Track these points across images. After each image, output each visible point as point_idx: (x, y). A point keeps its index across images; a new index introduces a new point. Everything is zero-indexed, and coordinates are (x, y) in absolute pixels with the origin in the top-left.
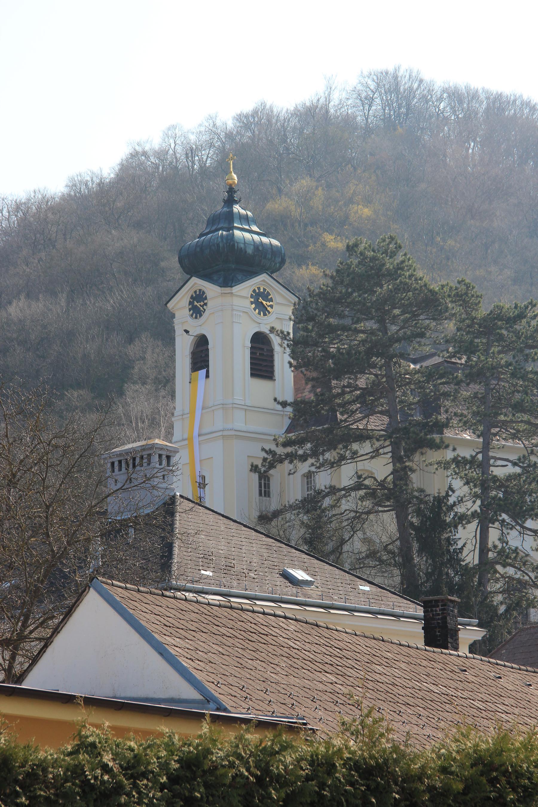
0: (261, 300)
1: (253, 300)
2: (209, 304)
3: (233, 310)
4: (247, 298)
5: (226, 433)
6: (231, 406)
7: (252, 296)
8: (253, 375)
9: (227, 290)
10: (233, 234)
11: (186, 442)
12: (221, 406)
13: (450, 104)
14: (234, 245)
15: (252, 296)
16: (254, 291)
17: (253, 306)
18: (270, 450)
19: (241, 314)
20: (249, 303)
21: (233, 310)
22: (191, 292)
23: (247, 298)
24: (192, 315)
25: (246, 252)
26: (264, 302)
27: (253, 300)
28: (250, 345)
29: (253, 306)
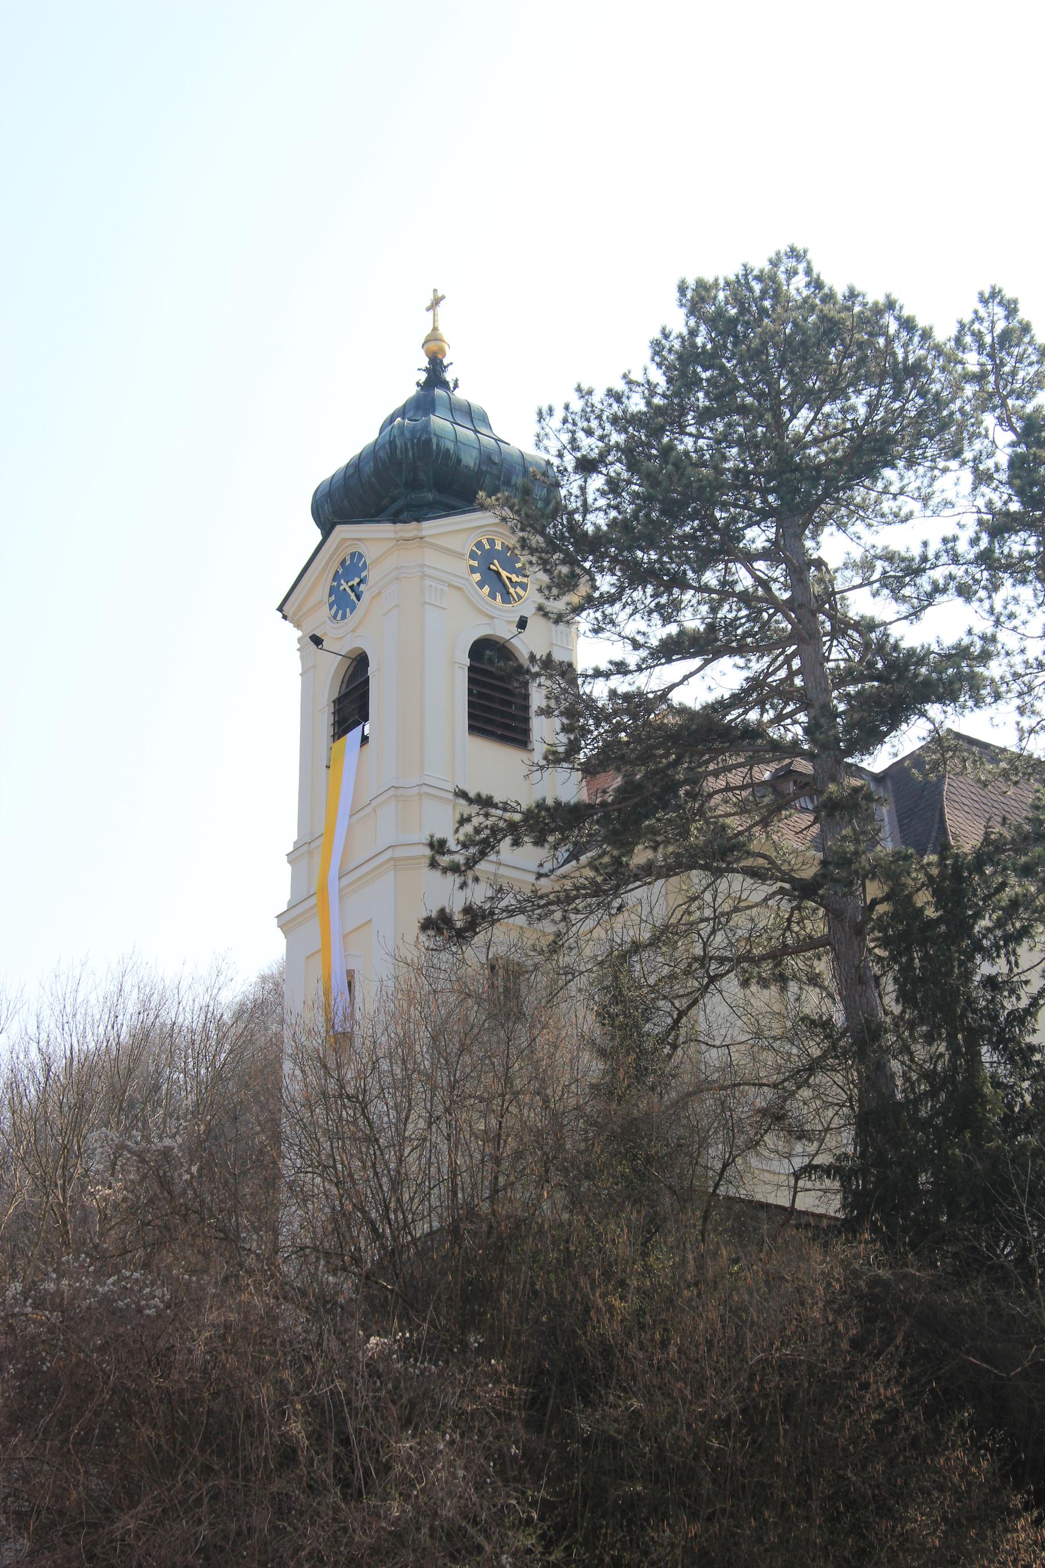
0: (496, 566)
1: (475, 563)
2: (371, 581)
3: (424, 576)
4: (460, 556)
5: (400, 853)
6: (416, 790)
7: (473, 555)
8: (473, 729)
9: (409, 529)
10: (427, 424)
11: (313, 901)
12: (392, 792)
13: (863, 1041)
14: (428, 442)
15: (473, 555)
16: (479, 545)
17: (477, 577)
18: (479, 795)
19: (446, 589)
20: (464, 571)
21: (424, 576)
22: (335, 566)
23: (460, 556)
24: (335, 617)
25: (459, 461)
26: (504, 574)
27: (475, 563)
28: (467, 662)
29: (477, 577)
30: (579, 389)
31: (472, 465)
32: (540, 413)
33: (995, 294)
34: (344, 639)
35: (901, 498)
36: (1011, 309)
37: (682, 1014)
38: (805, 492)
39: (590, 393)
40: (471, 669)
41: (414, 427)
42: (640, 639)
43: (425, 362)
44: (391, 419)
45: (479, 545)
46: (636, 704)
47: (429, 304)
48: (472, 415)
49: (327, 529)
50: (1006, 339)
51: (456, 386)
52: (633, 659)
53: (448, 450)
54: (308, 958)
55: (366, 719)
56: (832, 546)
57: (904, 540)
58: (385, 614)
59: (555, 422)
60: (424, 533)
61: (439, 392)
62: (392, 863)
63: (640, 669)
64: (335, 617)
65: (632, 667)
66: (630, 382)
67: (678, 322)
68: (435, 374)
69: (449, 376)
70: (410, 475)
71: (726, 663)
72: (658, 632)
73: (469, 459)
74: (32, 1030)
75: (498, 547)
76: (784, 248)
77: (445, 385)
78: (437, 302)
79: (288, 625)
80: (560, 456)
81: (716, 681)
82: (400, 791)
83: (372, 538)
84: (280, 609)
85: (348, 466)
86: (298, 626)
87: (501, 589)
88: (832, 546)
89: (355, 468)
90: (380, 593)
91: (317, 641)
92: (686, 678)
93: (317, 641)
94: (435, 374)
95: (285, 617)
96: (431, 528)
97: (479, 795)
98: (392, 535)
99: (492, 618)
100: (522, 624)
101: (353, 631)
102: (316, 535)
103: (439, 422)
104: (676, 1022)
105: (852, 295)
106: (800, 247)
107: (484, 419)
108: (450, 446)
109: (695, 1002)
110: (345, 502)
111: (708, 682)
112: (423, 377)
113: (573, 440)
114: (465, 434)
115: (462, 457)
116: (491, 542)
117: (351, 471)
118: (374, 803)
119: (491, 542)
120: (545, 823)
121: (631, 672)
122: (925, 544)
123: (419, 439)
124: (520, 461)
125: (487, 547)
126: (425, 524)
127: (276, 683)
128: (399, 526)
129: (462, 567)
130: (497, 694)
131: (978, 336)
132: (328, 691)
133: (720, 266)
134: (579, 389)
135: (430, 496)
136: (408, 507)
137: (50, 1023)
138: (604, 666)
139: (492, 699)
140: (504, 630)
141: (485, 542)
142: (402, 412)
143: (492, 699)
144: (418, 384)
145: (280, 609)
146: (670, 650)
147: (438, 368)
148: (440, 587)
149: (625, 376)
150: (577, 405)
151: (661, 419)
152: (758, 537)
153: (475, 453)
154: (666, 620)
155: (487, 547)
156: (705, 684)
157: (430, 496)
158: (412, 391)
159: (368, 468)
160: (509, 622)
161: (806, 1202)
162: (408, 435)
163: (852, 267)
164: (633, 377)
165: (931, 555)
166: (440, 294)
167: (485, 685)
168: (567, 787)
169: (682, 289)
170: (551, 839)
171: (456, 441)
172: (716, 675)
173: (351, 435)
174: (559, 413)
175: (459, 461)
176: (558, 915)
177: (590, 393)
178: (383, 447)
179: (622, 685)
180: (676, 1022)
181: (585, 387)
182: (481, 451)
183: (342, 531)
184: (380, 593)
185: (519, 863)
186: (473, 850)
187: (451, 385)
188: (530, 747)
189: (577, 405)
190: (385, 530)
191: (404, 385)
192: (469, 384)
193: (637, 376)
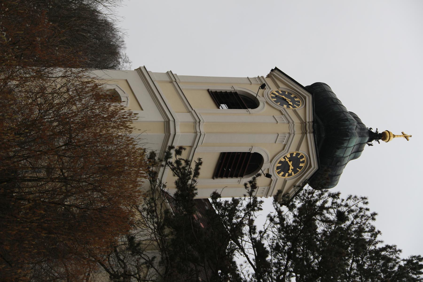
1: (294, 155)
4: (298, 149)
9: (309, 128)
12: (198, 120)
14: (347, 136)
15: (298, 154)
18: (199, 169)
19: (284, 143)
23: (298, 149)
24: (273, 93)
27: (294, 155)
31: (337, 154)
32: (365, 198)
39: (373, 219)
40: (249, 153)
41: (353, 129)
44: (356, 117)
47: (405, 133)
49: (309, 89)
51: (369, 145)
53: (343, 144)
54: (126, 81)
58: (273, 116)
59: (361, 205)
60: (308, 135)
62: (167, 120)
64: (273, 93)
69: (374, 142)
72: (266, 243)
73: (339, 153)
77: (370, 140)
78: (406, 137)
82: (198, 124)
83: (306, 111)
84: (276, 68)
85: (337, 99)
86: (268, 76)
87: (283, 168)
90: (282, 114)
95: (272, 70)
97: (199, 169)
98: (307, 120)
99: (271, 162)
101: (267, 102)
103: (355, 141)
107: (355, 157)
108: (345, 145)
110: (320, 95)
111: (244, 265)
112: (374, 131)
114: (349, 151)
115: (340, 150)
117: (335, 101)
118: (193, 112)
119: (303, 162)
121: (251, 235)
123: (348, 132)
124: (337, 174)
125: (301, 160)
126: (312, 135)
127: (243, 68)
130: (238, 164)
134: (375, 214)
135: (323, 136)
141: (303, 159)
142: (359, 122)
144: (371, 128)
145: (276, 68)
147: (378, 137)
148: (285, 141)
149: (379, 232)
150: (368, 213)
153: (342, 155)
155: (301, 160)
158: (368, 126)
160: (268, 169)
162: (350, 127)
164: (379, 236)
166: (409, 138)
171: (347, 148)
173: (350, 100)
175: (338, 148)
177: (373, 219)
178: (345, 116)
181: (376, 217)
182: (343, 157)
184: (282, 114)
187: (370, 143)
188: (215, 178)
189: (368, 213)
191: (371, 123)
192: (372, 151)
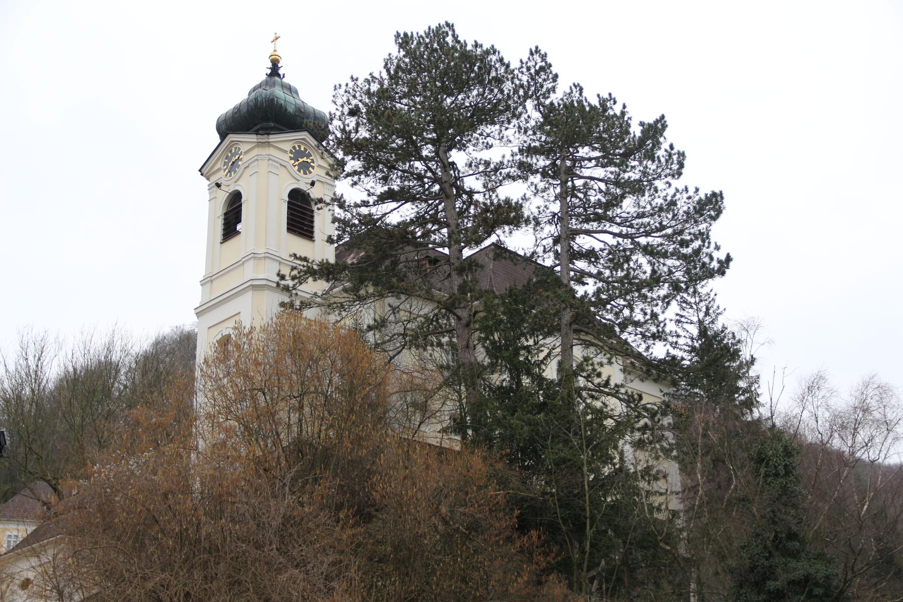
4: (286, 152)
7: (291, 152)
8: (289, 230)
9: (264, 139)
15: (291, 152)
20: (287, 159)
23: (286, 152)
30: (352, 77)
33: (537, 50)
34: (230, 187)
35: (488, 139)
36: (544, 57)
37: (392, 358)
38: (454, 129)
39: (357, 79)
40: (289, 203)
42: (372, 191)
43: (270, 65)
44: (254, 89)
45: (294, 147)
46: (368, 220)
48: (289, 89)
50: (542, 69)
52: (371, 200)
55: (240, 221)
56: (457, 157)
57: (495, 155)
59: (342, 91)
61: (277, 78)
63: (374, 205)
65: (371, 203)
66: (373, 77)
67: (396, 52)
68: (275, 71)
69: (281, 72)
70: (265, 116)
71: (409, 205)
72: (380, 189)
73: (291, 109)
74: (70, 356)
75: (302, 149)
76: (443, 23)
77: (279, 75)
79: (203, 178)
80: (342, 106)
81: (407, 212)
83: (245, 141)
84: (200, 170)
86: (208, 179)
87: (305, 167)
88: (457, 157)
89: (238, 110)
91: (218, 185)
92: (392, 211)
93: (218, 185)
94: (275, 71)
95: (202, 175)
96: (273, 138)
100: (313, 184)
102: (217, 139)
103: (279, 92)
104: (389, 362)
105: (476, 45)
106: (451, 22)
107: (297, 93)
108: (283, 102)
109: (399, 352)
110: (235, 124)
111: (401, 213)
112: (269, 71)
113: (348, 100)
114: (290, 98)
116: (299, 147)
119: (299, 147)
120: (326, 271)
122: (504, 157)
126: (271, 136)
128: (259, 136)
129: (286, 157)
130: (300, 214)
131: (528, 69)
132: (220, 210)
133: (418, 27)
134: (352, 77)
135: (272, 124)
136: (262, 129)
137: (78, 355)
138: (359, 202)
139: (300, 217)
140: (304, 186)
142: (260, 86)
143: (300, 217)
145: (200, 170)
146: (389, 196)
151: (384, 94)
152: (427, 151)
154: (384, 184)
156: (399, 214)
157: (272, 124)
158: (264, 77)
159: (244, 110)
161: (446, 444)
163: (470, 33)
164: (374, 75)
165: (506, 162)
167: (294, 210)
168: (329, 254)
169: (398, 35)
170: (637, 281)
171: (285, 101)
172: (405, 210)
173: (235, 95)
174: (344, 87)
176: (337, 313)
177: (357, 79)
179: (364, 211)
180: (389, 362)
181: (355, 77)
183: (232, 137)
185: (314, 287)
186: (296, 281)
189: (351, 84)
190: (253, 138)
193: (376, 75)
